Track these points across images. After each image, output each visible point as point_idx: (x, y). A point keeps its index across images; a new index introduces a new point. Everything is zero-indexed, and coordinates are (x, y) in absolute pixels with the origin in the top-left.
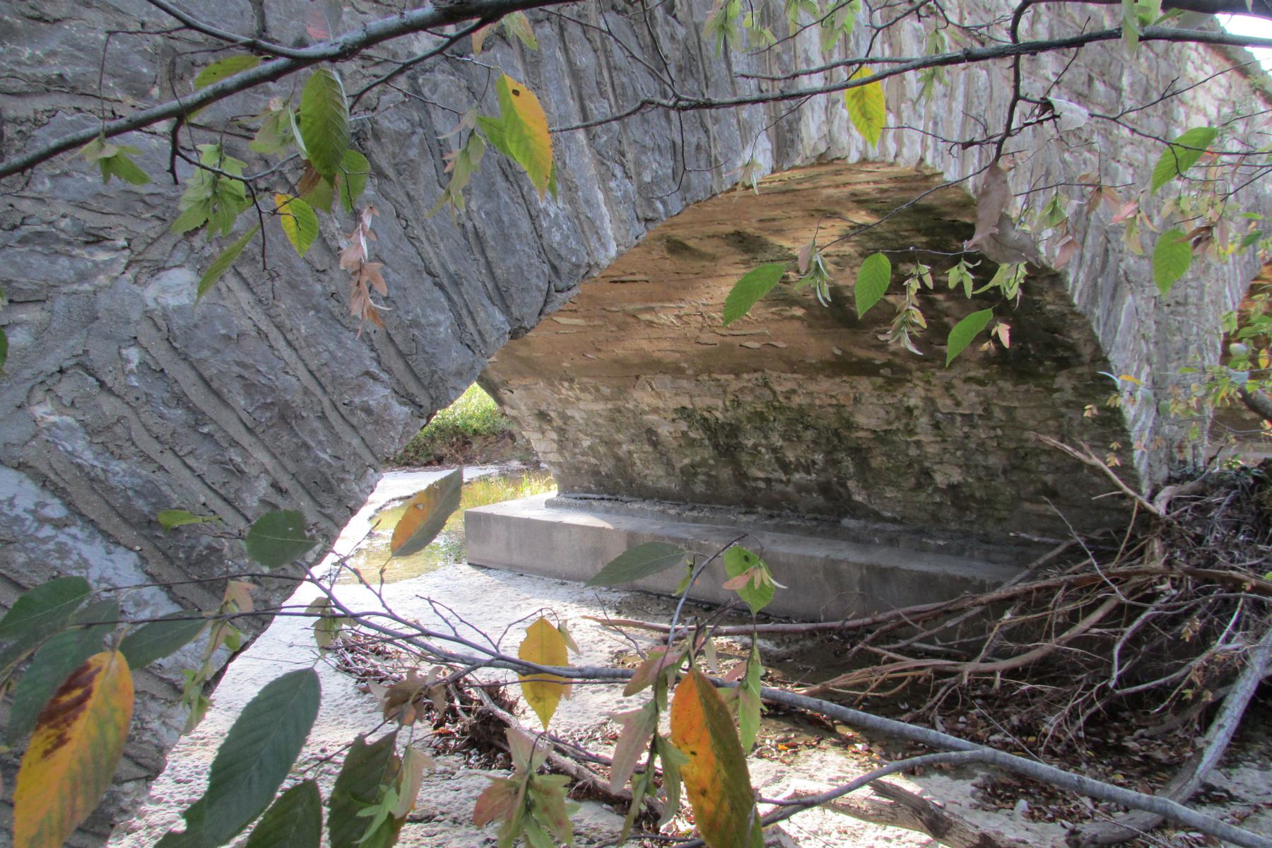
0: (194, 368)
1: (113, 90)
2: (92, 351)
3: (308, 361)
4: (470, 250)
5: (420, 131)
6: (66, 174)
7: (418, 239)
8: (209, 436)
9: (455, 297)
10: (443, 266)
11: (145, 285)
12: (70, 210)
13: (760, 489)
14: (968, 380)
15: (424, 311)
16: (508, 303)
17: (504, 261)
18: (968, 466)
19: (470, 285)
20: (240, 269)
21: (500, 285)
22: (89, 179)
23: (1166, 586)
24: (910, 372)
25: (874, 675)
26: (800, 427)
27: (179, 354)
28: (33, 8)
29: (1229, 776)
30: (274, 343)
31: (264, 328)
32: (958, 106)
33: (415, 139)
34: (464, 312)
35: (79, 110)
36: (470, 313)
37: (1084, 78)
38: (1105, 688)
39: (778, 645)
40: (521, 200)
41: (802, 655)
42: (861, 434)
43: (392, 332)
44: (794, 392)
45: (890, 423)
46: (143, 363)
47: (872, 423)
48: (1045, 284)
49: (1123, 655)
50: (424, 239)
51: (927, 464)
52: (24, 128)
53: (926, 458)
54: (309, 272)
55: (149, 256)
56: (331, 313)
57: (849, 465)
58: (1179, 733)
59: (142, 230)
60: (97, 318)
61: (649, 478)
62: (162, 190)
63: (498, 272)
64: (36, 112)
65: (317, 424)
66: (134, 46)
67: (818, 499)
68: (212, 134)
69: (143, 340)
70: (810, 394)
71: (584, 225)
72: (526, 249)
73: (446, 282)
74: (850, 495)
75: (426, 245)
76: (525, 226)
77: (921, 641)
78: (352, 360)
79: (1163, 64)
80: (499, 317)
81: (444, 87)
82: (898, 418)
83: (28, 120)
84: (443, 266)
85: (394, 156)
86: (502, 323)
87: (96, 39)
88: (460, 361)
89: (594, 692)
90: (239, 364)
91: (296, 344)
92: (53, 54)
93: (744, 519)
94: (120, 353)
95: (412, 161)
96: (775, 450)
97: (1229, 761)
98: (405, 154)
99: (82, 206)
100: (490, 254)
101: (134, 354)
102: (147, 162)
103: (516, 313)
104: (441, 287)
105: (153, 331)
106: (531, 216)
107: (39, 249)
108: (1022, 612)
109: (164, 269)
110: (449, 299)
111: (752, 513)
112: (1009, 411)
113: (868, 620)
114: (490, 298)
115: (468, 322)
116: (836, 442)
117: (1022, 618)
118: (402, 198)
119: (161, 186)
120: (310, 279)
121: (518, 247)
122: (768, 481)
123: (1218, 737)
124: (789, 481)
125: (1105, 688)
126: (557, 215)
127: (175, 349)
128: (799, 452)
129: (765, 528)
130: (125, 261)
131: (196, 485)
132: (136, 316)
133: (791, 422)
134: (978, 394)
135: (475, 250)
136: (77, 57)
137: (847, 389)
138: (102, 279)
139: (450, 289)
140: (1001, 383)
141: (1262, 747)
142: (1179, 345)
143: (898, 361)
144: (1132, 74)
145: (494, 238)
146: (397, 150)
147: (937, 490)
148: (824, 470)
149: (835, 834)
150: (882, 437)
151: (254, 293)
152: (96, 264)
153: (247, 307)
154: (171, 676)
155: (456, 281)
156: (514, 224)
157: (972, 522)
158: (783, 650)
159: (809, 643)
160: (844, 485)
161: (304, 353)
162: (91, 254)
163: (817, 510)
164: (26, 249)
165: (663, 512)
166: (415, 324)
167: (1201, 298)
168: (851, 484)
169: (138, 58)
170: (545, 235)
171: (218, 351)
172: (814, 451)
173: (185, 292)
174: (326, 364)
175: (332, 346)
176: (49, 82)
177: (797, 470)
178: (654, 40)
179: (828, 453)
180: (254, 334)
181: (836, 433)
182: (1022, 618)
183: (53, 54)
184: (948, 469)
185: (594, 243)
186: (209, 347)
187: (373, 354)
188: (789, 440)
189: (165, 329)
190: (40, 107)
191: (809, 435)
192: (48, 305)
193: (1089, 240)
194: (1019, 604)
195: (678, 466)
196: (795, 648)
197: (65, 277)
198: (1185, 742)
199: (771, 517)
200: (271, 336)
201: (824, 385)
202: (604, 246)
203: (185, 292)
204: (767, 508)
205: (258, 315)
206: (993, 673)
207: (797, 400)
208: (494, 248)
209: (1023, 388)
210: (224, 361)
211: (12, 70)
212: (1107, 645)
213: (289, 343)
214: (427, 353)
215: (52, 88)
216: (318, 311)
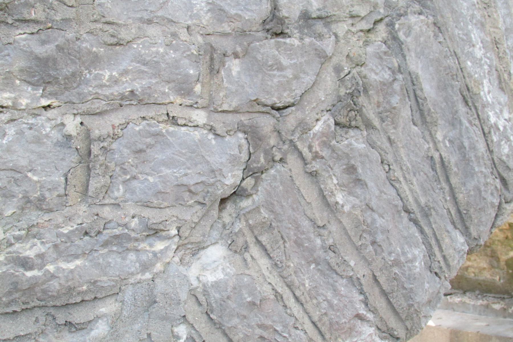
0: (225, 334)
1: (168, 95)
2: (154, 334)
3: (312, 314)
4: (438, 181)
5: (400, 77)
6: (134, 178)
7: (398, 180)
9: (426, 229)
10: (416, 201)
11: (188, 265)
15: (402, 249)
16: (467, 224)
17: (464, 184)
19: (437, 214)
20: (260, 238)
21: (461, 209)
22: (151, 179)
27: (215, 324)
28: (112, 36)
30: (287, 302)
31: (279, 290)
33: (397, 86)
34: (433, 242)
35: (144, 118)
36: (437, 240)
40: (477, 122)
43: (377, 274)
50: (401, 179)
52: (105, 144)
54: (312, 229)
55: (193, 239)
56: (329, 264)
59: (188, 218)
60: (155, 302)
61: (471, 270)
62: (203, 179)
63: (460, 197)
64: (114, 127)
66: (184, 52)
68: (238, 115)
69: (190, 318)
72: (484, 170)
73: (419, 216)
75: (403, 183)
76: (481, 147)
78: (346, 306)
81: (417, 28)
83: (109, 136)
84: (416, 201)
85: (379, 105)
86: (462, 244)
87: (157, 53)
88: (431, 291)
90: (261, 326)
91: (302, 298)
92: (125, 72)
94: (172, 332)
95: (394, 108)
98: (389, 102)
99: (147, 205)
100: (454, 180)
102: (194, 155)
103: (474, 234)
104: (415, 222)
105: (196, 308)
106: (484, 134)
107: (115, 248)
109: (204, 248)
110: (422, 231)
114: (453, 223)
115: (436, 249)
118: (386, 145)
119: (203, 175)
120: (312, 236)
121: (477, 169)
126: (505, 127)
127: (212, 319)
130: (174, 247)
132: (184, 296)
135: (441, 179)
136: (143, 72)
138: (159, 267)
139: (422, 223)
145: (456, 165)
146: (381, 100)
151: (270, 258)
152: (155, 254)
153: (267, 274)
156: (473, 148)
161: (309, 307)
162: (151, 245)
164: (106, 250)
165: (487, 306)
166: (397, 263)
169: (187, 61)
170: (496, 150)
171: (245, 317)
173: (220, 267)
174: (326, 314)
175: (329, 295)
176: (123, 97)
180: (272, 297)
183: (125, 72)
186: (238, 315)
187: (362, 297)
189: (204, 303)
190: (117, 122)
192: (119, 297)
195: (504, 258)
197: (133, 269)
200: (285, 297)
203: (220, 267)
205: (275, 280)
208: (456, 174)
210: (249, 326)
211: (96, 93)
213: (297, 299)
214: (405, 288)
215: (124, 103)
216: (317, 264)
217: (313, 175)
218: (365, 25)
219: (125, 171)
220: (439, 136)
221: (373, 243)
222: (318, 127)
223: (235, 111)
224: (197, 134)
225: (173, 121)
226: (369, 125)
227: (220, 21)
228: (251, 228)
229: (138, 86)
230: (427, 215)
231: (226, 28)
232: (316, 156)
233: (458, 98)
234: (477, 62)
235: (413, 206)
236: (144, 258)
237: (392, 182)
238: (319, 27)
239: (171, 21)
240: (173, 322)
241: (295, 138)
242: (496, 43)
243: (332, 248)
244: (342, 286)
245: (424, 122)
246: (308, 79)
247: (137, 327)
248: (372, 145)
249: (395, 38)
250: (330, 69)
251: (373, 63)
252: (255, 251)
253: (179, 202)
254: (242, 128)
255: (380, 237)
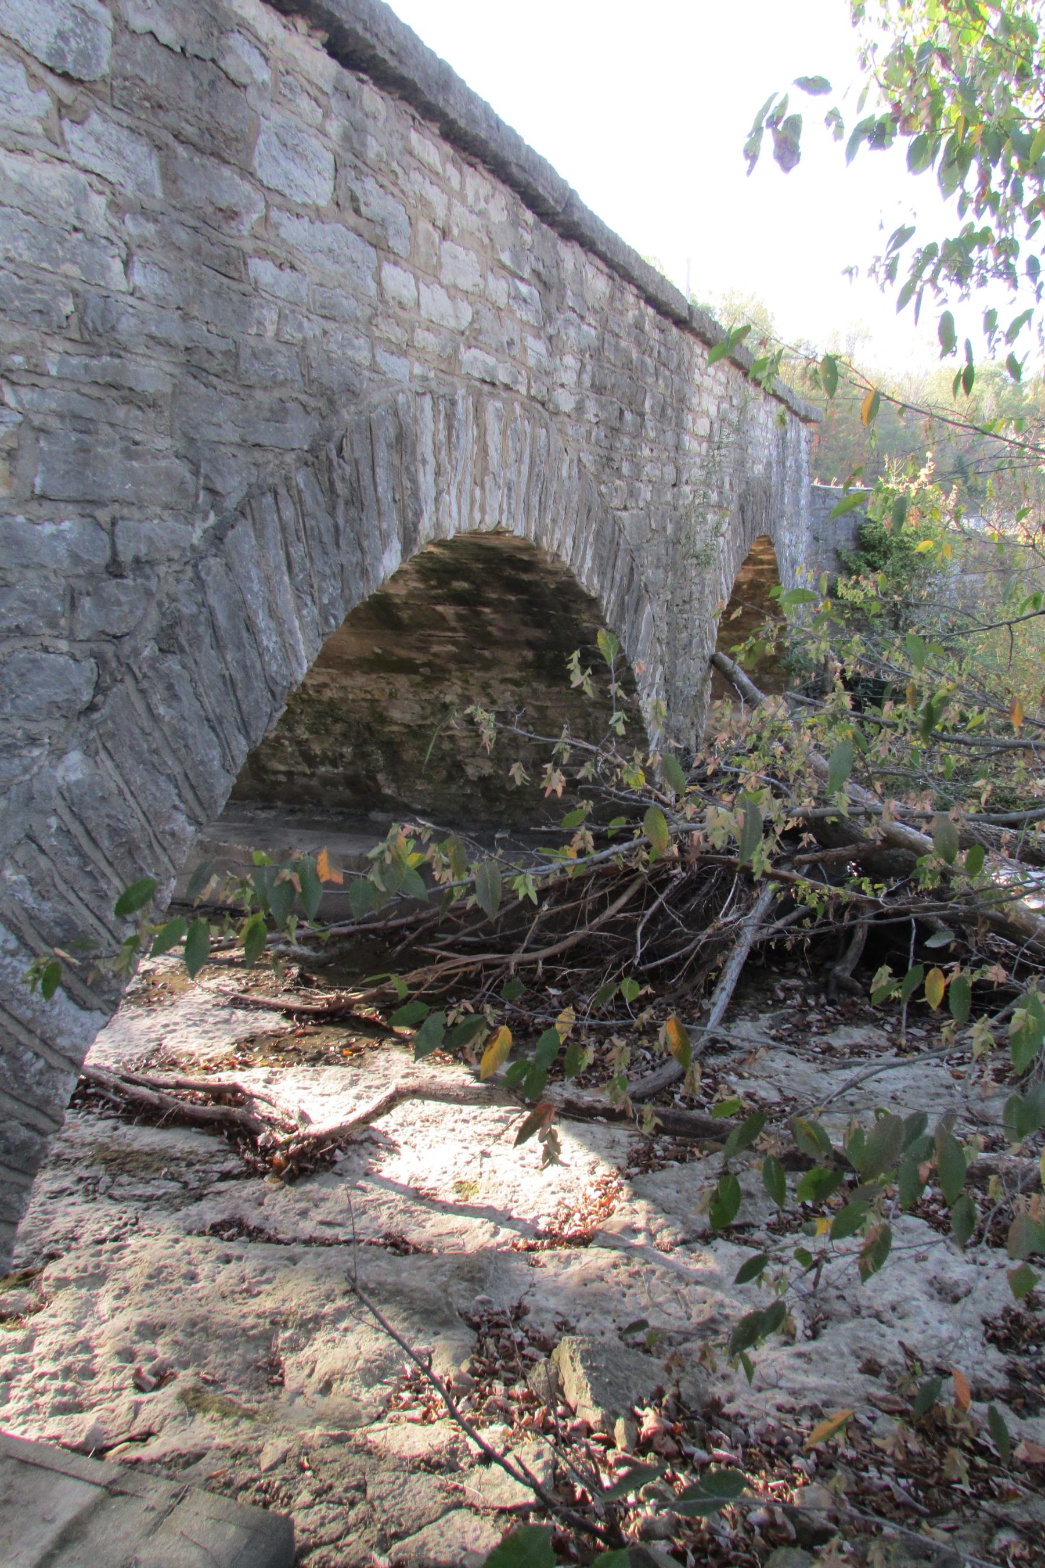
8: (90, 873)
12: (22, 723)
13: (280, 783)
14: (504, 681)
18: (499, 760)
23: (679, 870)
24: (449, 672)
25: (429, 975)
26: (329, 720)
29: (728, 1029)
32: (525, 468)
37: (617, 413)
38: (631, 965)
39: (315, 949)
41: (342, 958)
42: (395, 728)
44: (325, 685)
45: (425, 718)
46: (59, 828)
47: (407, 718)
48: (584, 606)
49: (644, 935)
51: (459, 758)
53: (459, 752)
57: (379, 758)
58: (689, 997)
63: (244, 707)
65: (147, 852)
67: (344, 792)
70: (344, 688)
71: (288, 650)
74: (379, 787)
76: (258, 665)
77: (468, 935)
79: (676, 379)
80: (243, 742)
82: (433, 714)
89: (132, 1018)
90: (108, 816)
92: (11, 609)
93: (262, 815)
96: (299, 743)
97: (729, 1017)
99: (28, 719)
100: (240, 694)
101: (53, 821)
104: (213, 729)
108: (557, 902)
111: (271, 808)
112: (541, 709)
113: (410, 919)
116: (367, 735)
117: (559, 908)
122: (290, 774)
123: (721, 998)
124: (313, 775)
125: (631, 965)
128: (326, 745)
129: (287, 824)
131: (86, 913)
133: (320, 715)
134: (513, 693)
137: (383, 684)
138: (35, 769)
140: (535, 685)
141: (752, 1001)
142: (685, 641)
143: (438, 661)
144: (653, 397)
147: (468, 782)
148: (351, 763)
149: (419, 1124)
150: (417, 733)
154: (70, 1054)
155: (220, 720)
156: (254, 667)
157: (501, 813)
158: (321, 954)
159: (347, 945)
160: (374, 779)
163: (342, 803)
166: (202, 762)
167: (702, 593)
168: (380, 777)
172: (342, 744)
175: (154, 789)
176: (9, 630)
177: (323, 763)
178: (332, 483)
179: (357, 746)
181: (368, 727)
182: (559, 908)
183: (11, 609)
184: (480, 761)
185: (295, 665)
188: (317, 733)
191: (338, 728)
193: (619, 562)
194: (554, 895)
196: (334, 951)
198: (694, 1004)
199: (292, 812)
201: (359, 680)
202: (300, 665)
204: (287, 801)
206: (536, 962)
207: (328, 694)
209: (556, 689)
212: (629, 927)
217: (142, 692)
218: (176, 567)
219: (12, 692)
220: (229, 657)
221: (186, 746)
222: (146, 653)
223: (88, 640)
224: (62, 660)
225: (46, 649)
226: (182, 650)
227: (76, 565)
228: (101, 736)
229: (22, 620)
230: (220, 723)
231: (80, 571)
232: (145, 676)
233: (242, 626)
234: (255, 595)
235: (212, 716)
236: (25, 762)
237: (197, 696)
238: (148, 570)
239: (43, 566)
240: (45, 813)
241: (131, 661)
242: (268, 578)
243: (156, 752)
244: (162, 781)
245: (219, 647)
246: (139, 613)
247: (20, 819)
248: (184, 667)
249: (199, 578)
250: (154, 604)
251: (184, 599)
252: (103, 755)
253: (50, 715)
254: (93, 655)
255: (190, 742)
